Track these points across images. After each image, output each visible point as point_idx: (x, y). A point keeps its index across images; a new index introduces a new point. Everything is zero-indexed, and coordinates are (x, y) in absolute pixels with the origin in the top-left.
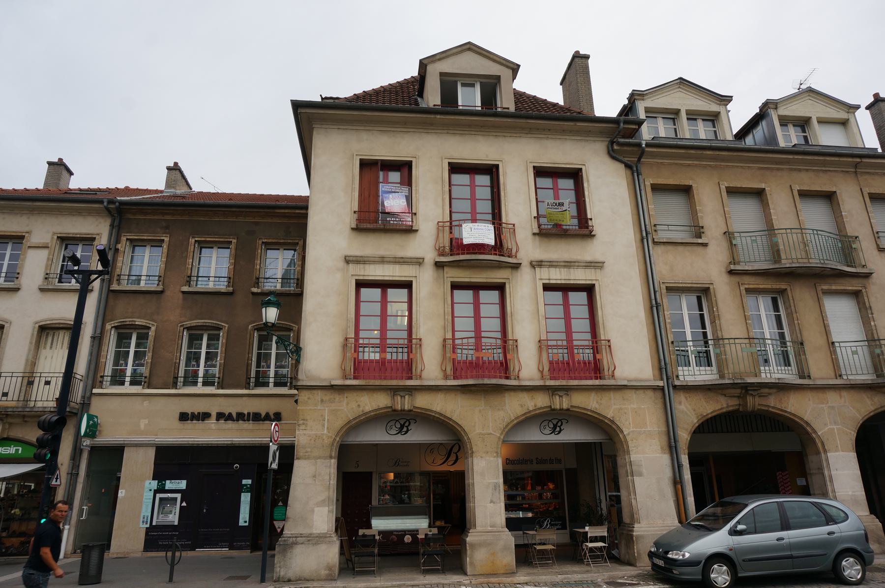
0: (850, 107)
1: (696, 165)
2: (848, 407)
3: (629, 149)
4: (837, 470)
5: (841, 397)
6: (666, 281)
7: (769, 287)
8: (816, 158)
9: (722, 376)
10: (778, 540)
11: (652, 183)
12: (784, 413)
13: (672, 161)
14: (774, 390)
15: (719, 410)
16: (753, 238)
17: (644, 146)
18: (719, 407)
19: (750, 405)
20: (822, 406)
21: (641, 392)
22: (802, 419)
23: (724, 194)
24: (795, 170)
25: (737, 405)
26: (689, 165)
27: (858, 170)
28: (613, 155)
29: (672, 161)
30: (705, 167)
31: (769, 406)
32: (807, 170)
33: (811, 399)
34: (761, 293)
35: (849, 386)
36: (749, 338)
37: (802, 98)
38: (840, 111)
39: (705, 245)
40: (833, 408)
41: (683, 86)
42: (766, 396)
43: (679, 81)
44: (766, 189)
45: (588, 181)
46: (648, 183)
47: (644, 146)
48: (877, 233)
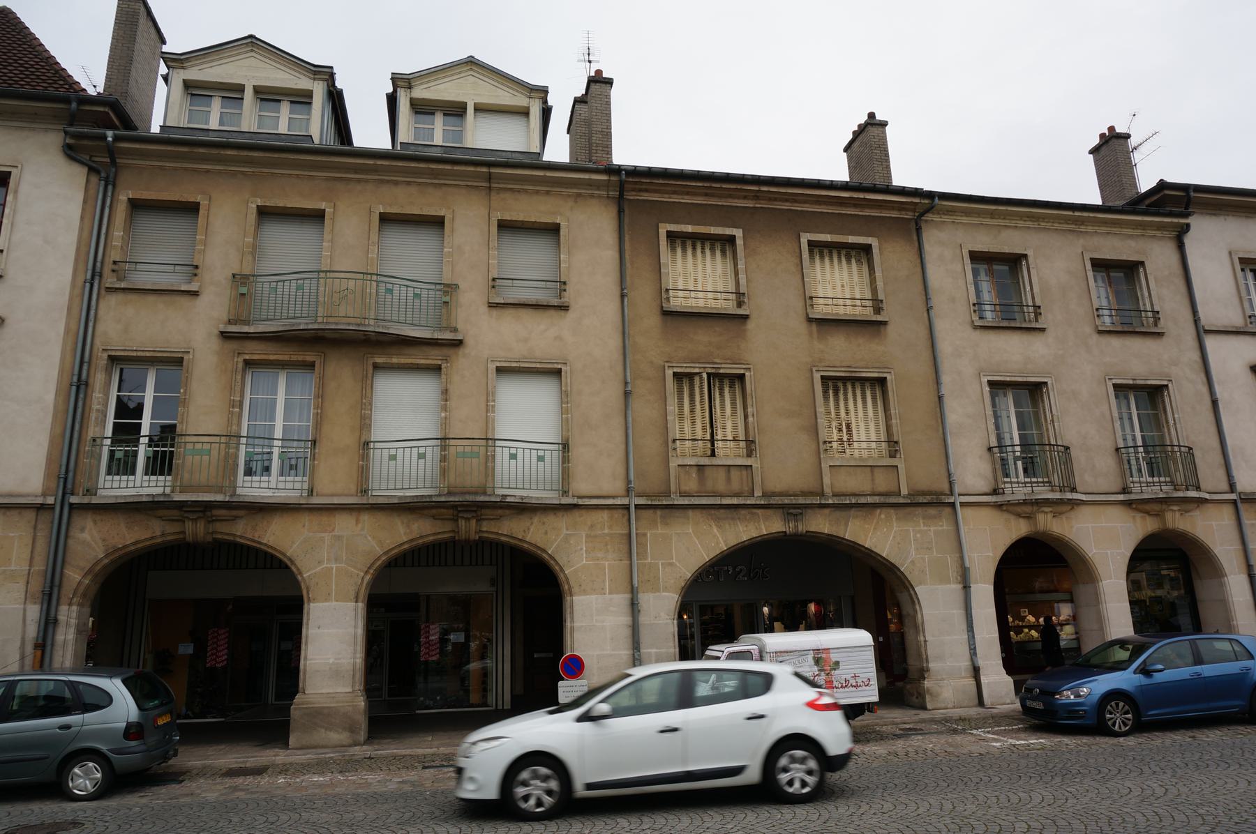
0: (531, 89)
1: (219, 172)
2: (366, 537)
3: (94, 144)
4: (319, 628)
5: (357, 522)
6: (109, 348)
7: (286, 358)
8: (413, 164)
9: (565, 493)
10: (61, 728)
11: (131, 197)
12: (258, 546)
13: (179, 165)
14: (507, 512)
15: (147, 539)
16: (300, 282)
17: (110, 139)
18: (148, 535)
19: (189, 535)
20: (323, 535)
21: (15, 512)
22: (284, 555)
23: (494, 229)
24: (388, 182)
25: (450, 532)
26: (208, 171)
27: (493, 185)
28: (71, 152)
29: (179, 165)
30: (234, 174)
31: (234, 535)
32: (408, 183)
33: (307, 524)
34: (286, 367)
35: (368, 506)
36: (487, 439)
37: (460, 73)
38: (516, 94)
39: (1043, 330)
40: (339, 538)
41: (258, 49)
42: (498, 519)
43: (249, 40)
44: (873, 244)
45: (16, 192)
46: (123, 199)
47: (110, 139)
48: (811, 298)
